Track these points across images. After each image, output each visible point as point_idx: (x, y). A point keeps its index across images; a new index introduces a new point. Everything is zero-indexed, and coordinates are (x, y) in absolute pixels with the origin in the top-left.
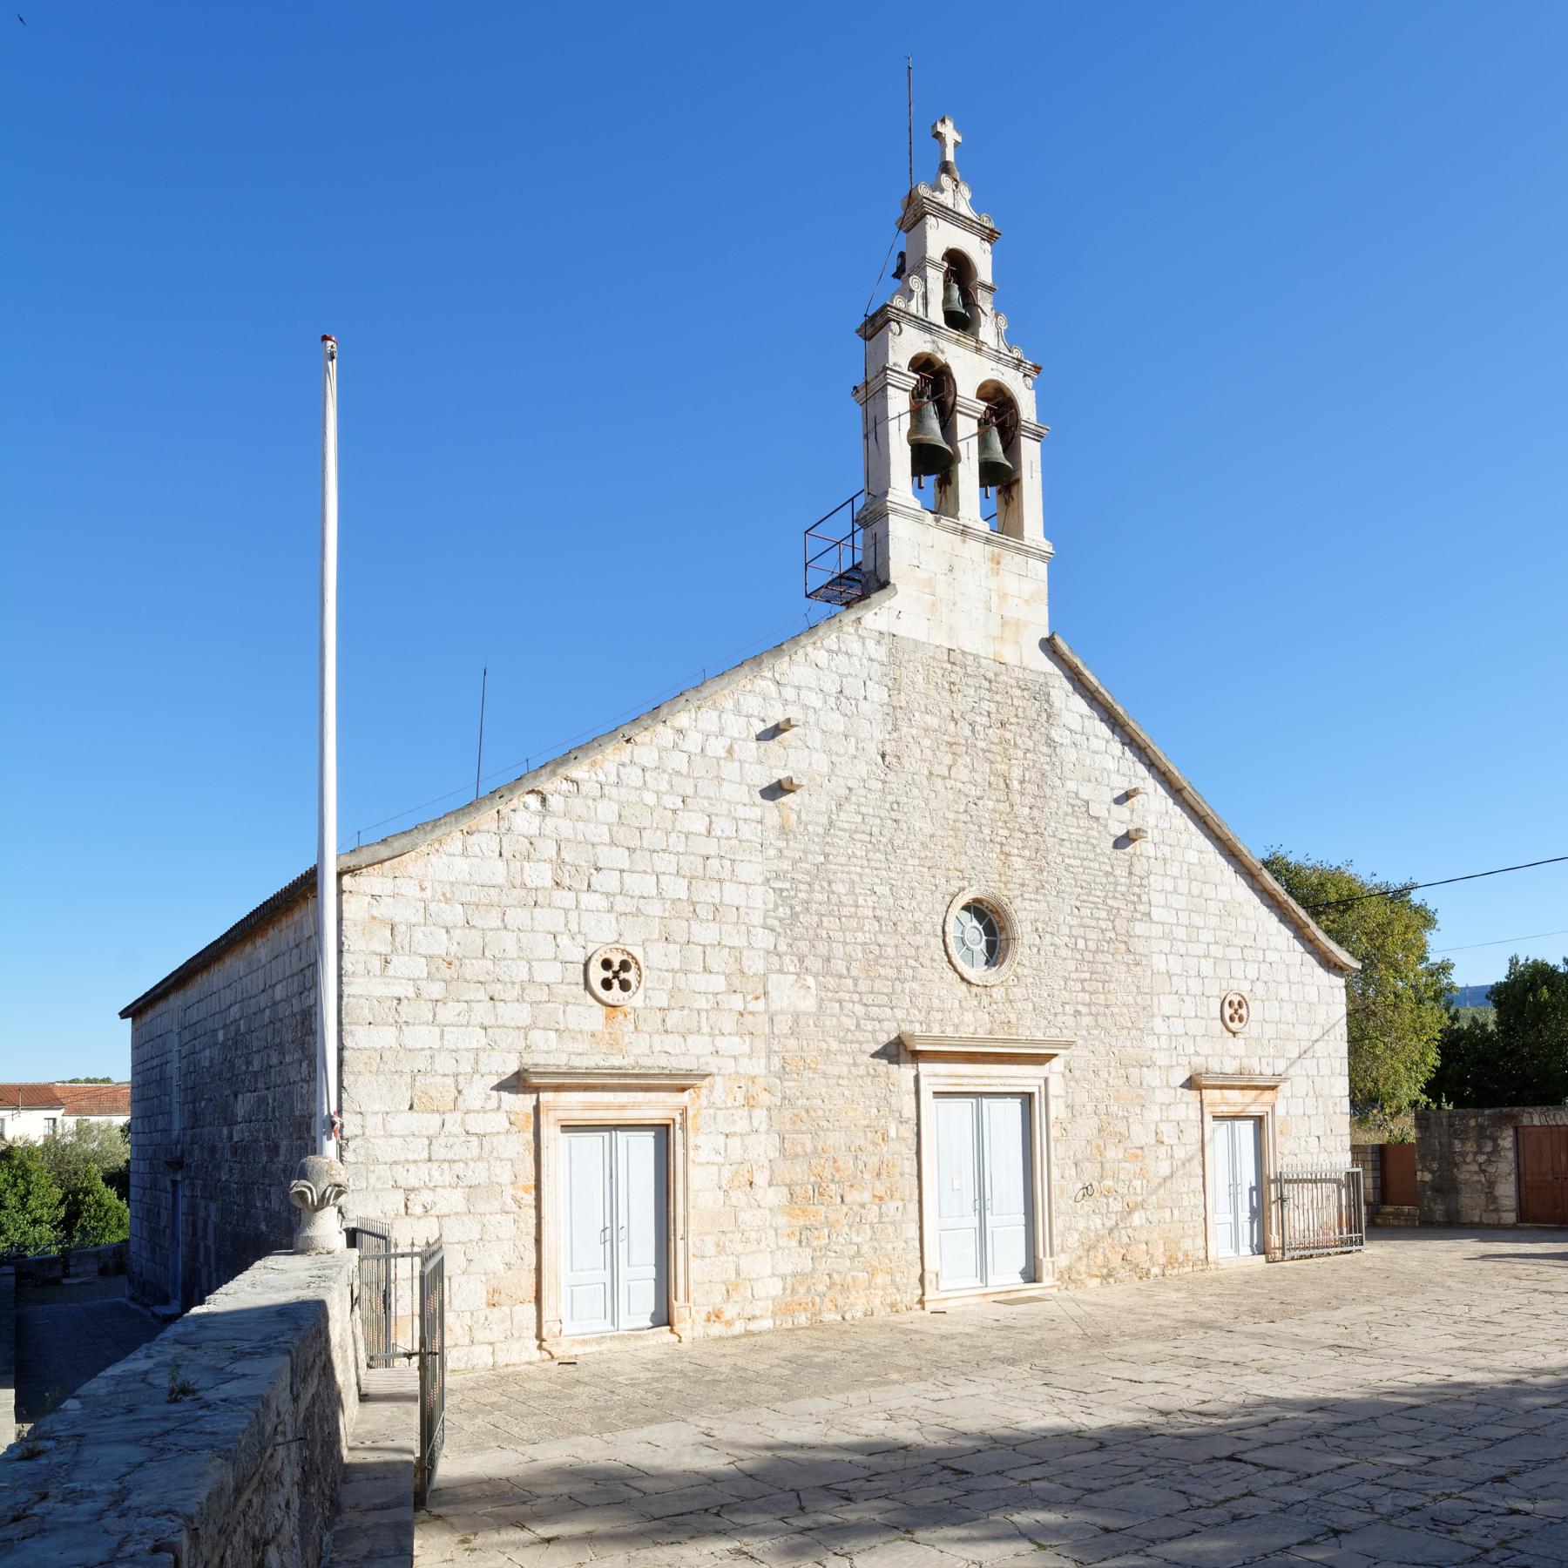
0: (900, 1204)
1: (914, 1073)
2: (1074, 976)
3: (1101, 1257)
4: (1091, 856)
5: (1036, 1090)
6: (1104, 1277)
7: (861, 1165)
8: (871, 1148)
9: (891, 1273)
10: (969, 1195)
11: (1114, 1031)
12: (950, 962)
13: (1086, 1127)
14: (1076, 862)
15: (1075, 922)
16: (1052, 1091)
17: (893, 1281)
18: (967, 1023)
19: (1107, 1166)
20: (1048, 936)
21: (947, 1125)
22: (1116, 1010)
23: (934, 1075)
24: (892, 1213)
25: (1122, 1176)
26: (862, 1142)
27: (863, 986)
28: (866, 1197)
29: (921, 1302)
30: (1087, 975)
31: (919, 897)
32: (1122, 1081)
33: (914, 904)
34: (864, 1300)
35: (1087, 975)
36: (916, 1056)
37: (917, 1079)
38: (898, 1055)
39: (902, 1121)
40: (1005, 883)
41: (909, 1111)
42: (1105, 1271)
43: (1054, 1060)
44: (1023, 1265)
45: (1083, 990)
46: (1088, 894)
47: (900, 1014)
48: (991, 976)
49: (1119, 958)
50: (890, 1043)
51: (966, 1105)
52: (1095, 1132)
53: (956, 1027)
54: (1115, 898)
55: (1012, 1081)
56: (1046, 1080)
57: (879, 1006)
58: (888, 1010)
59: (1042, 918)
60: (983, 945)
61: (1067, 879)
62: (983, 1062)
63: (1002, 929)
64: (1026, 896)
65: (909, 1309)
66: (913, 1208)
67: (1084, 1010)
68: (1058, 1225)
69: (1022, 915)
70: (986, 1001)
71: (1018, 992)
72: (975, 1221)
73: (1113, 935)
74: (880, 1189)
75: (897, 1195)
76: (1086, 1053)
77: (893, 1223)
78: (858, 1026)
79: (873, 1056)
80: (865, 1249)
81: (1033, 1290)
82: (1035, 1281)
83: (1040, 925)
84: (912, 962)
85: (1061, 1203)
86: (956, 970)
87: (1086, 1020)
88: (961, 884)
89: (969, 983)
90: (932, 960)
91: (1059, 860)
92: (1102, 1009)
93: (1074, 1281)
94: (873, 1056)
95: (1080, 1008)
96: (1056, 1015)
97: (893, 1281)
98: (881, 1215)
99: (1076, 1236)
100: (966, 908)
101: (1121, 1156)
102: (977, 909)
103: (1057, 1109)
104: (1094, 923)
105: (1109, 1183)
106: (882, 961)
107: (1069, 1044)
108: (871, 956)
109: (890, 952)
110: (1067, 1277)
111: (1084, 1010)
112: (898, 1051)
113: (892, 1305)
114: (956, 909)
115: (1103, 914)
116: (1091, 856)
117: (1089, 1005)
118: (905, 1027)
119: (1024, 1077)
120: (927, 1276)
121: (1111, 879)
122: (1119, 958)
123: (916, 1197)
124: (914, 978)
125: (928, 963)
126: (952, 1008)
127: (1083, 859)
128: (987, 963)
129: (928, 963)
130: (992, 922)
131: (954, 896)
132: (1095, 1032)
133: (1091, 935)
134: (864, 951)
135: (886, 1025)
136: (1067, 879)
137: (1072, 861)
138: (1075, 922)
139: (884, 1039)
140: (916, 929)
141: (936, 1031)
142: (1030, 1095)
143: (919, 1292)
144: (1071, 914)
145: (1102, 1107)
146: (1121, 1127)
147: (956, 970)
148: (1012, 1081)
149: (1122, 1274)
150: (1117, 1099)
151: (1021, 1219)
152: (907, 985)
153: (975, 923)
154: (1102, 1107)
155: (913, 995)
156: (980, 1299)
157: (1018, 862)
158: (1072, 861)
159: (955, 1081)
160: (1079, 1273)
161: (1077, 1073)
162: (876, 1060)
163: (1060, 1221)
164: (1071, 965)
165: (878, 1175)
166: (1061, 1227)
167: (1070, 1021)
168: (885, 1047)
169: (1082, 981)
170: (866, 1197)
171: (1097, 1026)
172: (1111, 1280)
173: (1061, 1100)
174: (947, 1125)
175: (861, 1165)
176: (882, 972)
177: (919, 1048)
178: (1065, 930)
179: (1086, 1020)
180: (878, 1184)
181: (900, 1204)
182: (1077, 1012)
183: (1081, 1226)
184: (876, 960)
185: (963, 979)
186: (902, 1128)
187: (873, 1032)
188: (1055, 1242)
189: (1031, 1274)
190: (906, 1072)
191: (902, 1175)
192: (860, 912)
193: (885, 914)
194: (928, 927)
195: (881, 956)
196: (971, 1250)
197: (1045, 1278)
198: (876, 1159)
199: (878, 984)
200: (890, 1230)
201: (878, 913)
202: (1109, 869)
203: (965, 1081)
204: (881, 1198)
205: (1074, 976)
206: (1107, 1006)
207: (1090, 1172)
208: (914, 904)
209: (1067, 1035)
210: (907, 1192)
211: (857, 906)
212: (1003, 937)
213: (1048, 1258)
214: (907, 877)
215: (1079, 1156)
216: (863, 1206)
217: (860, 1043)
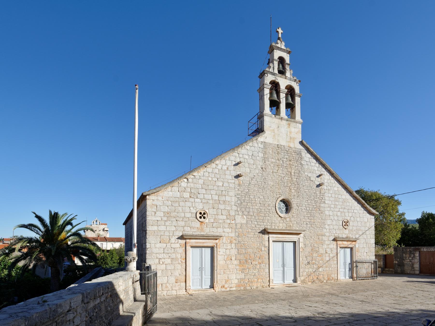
5: (296, 241)
6: (312, 282)
9: (262, 279)
10: (281, 263)
11: (316, 228)
13: (309, 249)
18: (281, 226)
23: (272, 237)
27: (257, 218)
28: (257, 263)
29: (269, 286)
36: (269, 233)
37: (269, 238)
41: (267, 244)
47: (265, 224)
51: (280, 244)
53: (278, 227)
58: (262, 223)
63: (289, 205)
66: (268, 265)
68: (301, 270)
70: (285, 221)
71: (293, 219)
74: (260, 261)
78: (255, 226)
79: (259, 233)
80: (256, 274)
81: (295, 284)
84: (268, 213)
85: (302, 266)
87: (309, 225)
94: (259, 233)
100: (281, 201)
102: (283, 201)
103: (301, 245)
105: (314, 261)
107: (304, 231)
109: (263, 210)
112: (264, 232)
113: (262, 286)
115: (314, 202)
118: (266, 227)
119: (294, 238)
124: (268, 216)
126: (277, 222)
130: (287, 204)
131: (278, 198)
133: (310, 206)
139: (261, 229)
141: (273, 227)
142: (295, 242)
145: (312, 245)
146: (317, 249)
149: (317, 281)
153: (283, 204)
154: (312, 245)
155: (268, 220)
157: (293, 191)
161: (307, 237)
164: (306, 213)
167: (305, 226)
170: (257, 263)
171: (312, 227)
176: (261, 215)
178: (304, 205)
182: (307, 224)
183: (307, 271)
184: (260, 213)
187: (259, 228)
189: (295, 281)
190: (266, 236)
193: (262, 202)
196: (281, 275)
199: (260, 218)
207: (309, 259)
209: (304, 229)
216: (256, 265)
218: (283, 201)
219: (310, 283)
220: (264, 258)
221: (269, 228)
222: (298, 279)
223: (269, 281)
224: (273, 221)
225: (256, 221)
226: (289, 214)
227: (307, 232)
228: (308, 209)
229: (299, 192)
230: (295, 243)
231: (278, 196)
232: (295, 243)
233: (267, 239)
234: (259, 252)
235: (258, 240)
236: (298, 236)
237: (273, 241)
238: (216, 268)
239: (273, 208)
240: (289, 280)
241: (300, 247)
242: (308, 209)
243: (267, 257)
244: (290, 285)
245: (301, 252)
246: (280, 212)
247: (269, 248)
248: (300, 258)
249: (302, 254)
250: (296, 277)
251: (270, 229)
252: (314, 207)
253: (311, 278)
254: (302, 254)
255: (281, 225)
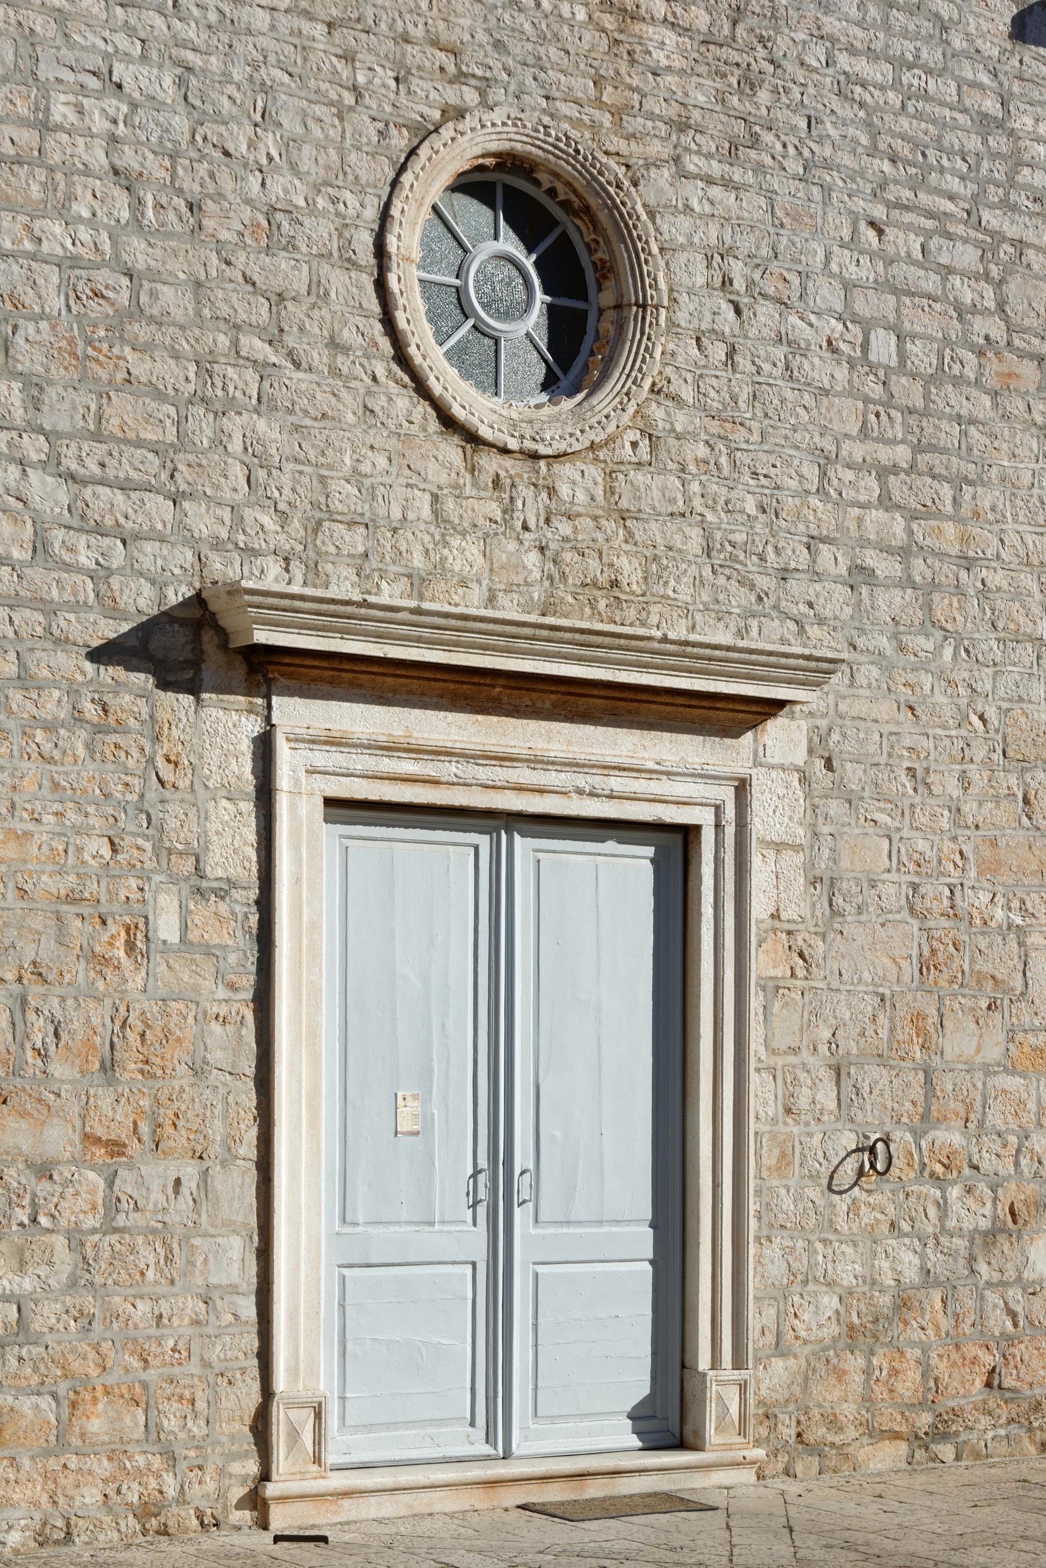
0: (190, 1173)
1: (253, 726)
2: (857, 451)
3: (913, 1375)
4: (931, 55)
5: (704, 818)
6: (920, 1441)
7: (39, 1031)
8: (81, 972)
9: (141, 1399)
10: (457, 1155)
11: (989, 646)
12: (402, 359)
13: (877, 953)
14: (879, 72)
15: (863, 271)
16: (764, 822)
17: (153, 1430)
18: (475, 573)
19: (946, 1083)
20: (766, 310)
21: (369, 929)
22: (997, 579)
23: (325, 739)
24: (157, 1197)
25: (995, 1119)
26: (47, 950)
27: (62, 411)
28: (59, 1139)
29: (256, 1502)
30: (902, 454)
31: (290, 124)
32: (1006, 813)
33: (270, 143)
34: (39, 1491)
35: (902, 454)
36: (265, 671)
37: (264, 749)
38: (196, 663)
39: (201, 888)
40: (618, 113)
41: (232, 852)
42: (925, 1420)
43: (774, 728)
44: (644, 1389)
45: (885, 501)
46: (917, 184)
47: (202, 520)
48: (557, 421)
49: (1016, 406)
50: (167, 618)
51: (457, 853)
52: (910, 970)
53: (418, 582)
54: (1009, 207)
55: (617, 783)
56: (742, 788)
57: (125, 487)
58: (160, 508)
59: (745, 244)
60: (535, 320)
61: (842, 125)
62: (515, 712)
63: (606, 270)
64: (693, 163)
65: (210, 1524)
66: (238, 1186)
67: (885, 567)
68: (766, 1264)
69: (675, 228)
70: (531, 505)
71: (651, 488)
72: (475, 1241)
73: (997, 330)
74: (112, 1115)
75: (177, 1139)
76: (885, 709)
77: (160, 1233)
78: (40, 547)
79: (100, 655)
80: (46, 1316)
81: (668, 1470)
82: (681, 1444)
83: (737, 269)
84: (256, 346)
85: (782, 1194)
86: (422, 390)
87: (891, 602)
88: (451, 95)
89: (472, 438)
90: (335, 345)
91: (816, 55)
92: (947, 572)
93: (816, 1450)
94: (100, 655)
95: (871, 558)
96: (784, 574)
97: (153, 1430)
98: (113, 1205)
99: (830, 1302)
100: (473, 184)
101: (994, 1053)
102: (507, 187)
103: (774, 886)
104: (931, 283)
105: (951, 1137)
106: (141, 331)
107: (817, 670)
108: (96, 309)
109: (173, 300)
110: (801, 1442)
111: (885, 567)
112: (193, 647)
113: (145, 1511)
114: (430, 182)
115: (967, 257)
116: (931, 55)
117: (904, 553)
118: (223, 568)
119: (669, 772)
120: (280, 1415)
121: (998, 142)
122: (1016, 406)
123: (248, 1149)
124: (263, 404)
125: (318, 356)
126: (404, 510)
127: (901, 64)
128: (549, 384)
129: (318, 356)
130: (569, 240)
131: (425, 132)
132: (923, 644)
133: (921, 321)
134: (71, 292)
135: (148, 553)
136: (842, 125)
137: (862, 67)
138: (863, 271)
139: (141, 601)
140: (274, 227)
141: (343, 586)
142: (689, 833)
143: (253, 1467)
144: (852, 244)
145: (935, 891)
146: (1000, 959)
147: (422, 390)
148: (617, 783)
149: (984, 1431)
150: (989, 868)
151: (642, 1240)
152: (235, 425)
153: (510, 244)
154: (935, 891)
155: (257, 460)
156: (477, 1499)
157: (664, 46)
158: (862, 67)
159: (408, 767)
160: (833, 1423)
161: (853, 774)
162: (111, 673)
163: (773, 1252)
164: (846, 416)
165: (109, 1067)
166: (776, 1270)
167: (836, 601)
168: (147, 630)
169: (884, 472)
170: (59, 1139)
171: (930, 623)
172: (946, 1451)
173: (793, 860)
174: (369, 929)
175: (39, 1031)
176: (141, 368)
177: (262, 636)
178: (827, 294)
179: (891, 602)
180: (104, 1099)
181: (190, 1173)
182: (860, 576)
183: (847, 1272)
184: (117, 327)
185: (448, 422)
186: (201, 913)
187: (101, 574)
188: (753, 1321)
189: (669, 1419)
190: (223, 725)
191: (198, 1071)
192: (57, 148)
193: (156, 168)
194: (320, 231)
195: (136, 311)
196: (457, 1339)
197: (711, 1433)
198: (99, 1015)
199: (122, 412)
200: (147, 1256)
201: (128, 158)
202: (991, 106)
203: (449, 769)
204: (116, 1148)
205: (857, 451)
206: (968, 563)
207: (886, 1097)
208: (270, 143)
209: (823, 642)
210: (217, 1130)
211: (45, 127)
212: (607, 298)
213: (728, 1373)
214: (245, 47)
215: (849, 1045)
216: (44, 1171)
217: (49, 609)
218: (507, 187)
219: (885, 1457)
220: (177, 1058)
221: (268, 579)
222: (721, 1395)
223: (261, 1427)
224: (345, 495)
225: (52, 463)
226: (604, 400)
227: (860, 705)
228: (883, 347)
229: (749, 84)
230: (675, 847)
231: (426, 98)
232: (675, 847)
233: (245, 769)
234: (102, 962)
235: (83, 772)
236: (731, 756)
237: (340, 808)
238: (509, 750)
239: (337, 280)
240: (583, 1406)
241: (759, 908)
242: (883, 347)
243: (231, 1046)
244: (595, 1490)
245: (773, 988)
246: (457, 356)
247: (265, 904)
248: (755, 1081)
249: (787, 1023)
250: (685, 1365)
251: (284, 606)
252: (980, 327)
253: (909, 1384)
254: (787, 1023)
255: (466, 555)
